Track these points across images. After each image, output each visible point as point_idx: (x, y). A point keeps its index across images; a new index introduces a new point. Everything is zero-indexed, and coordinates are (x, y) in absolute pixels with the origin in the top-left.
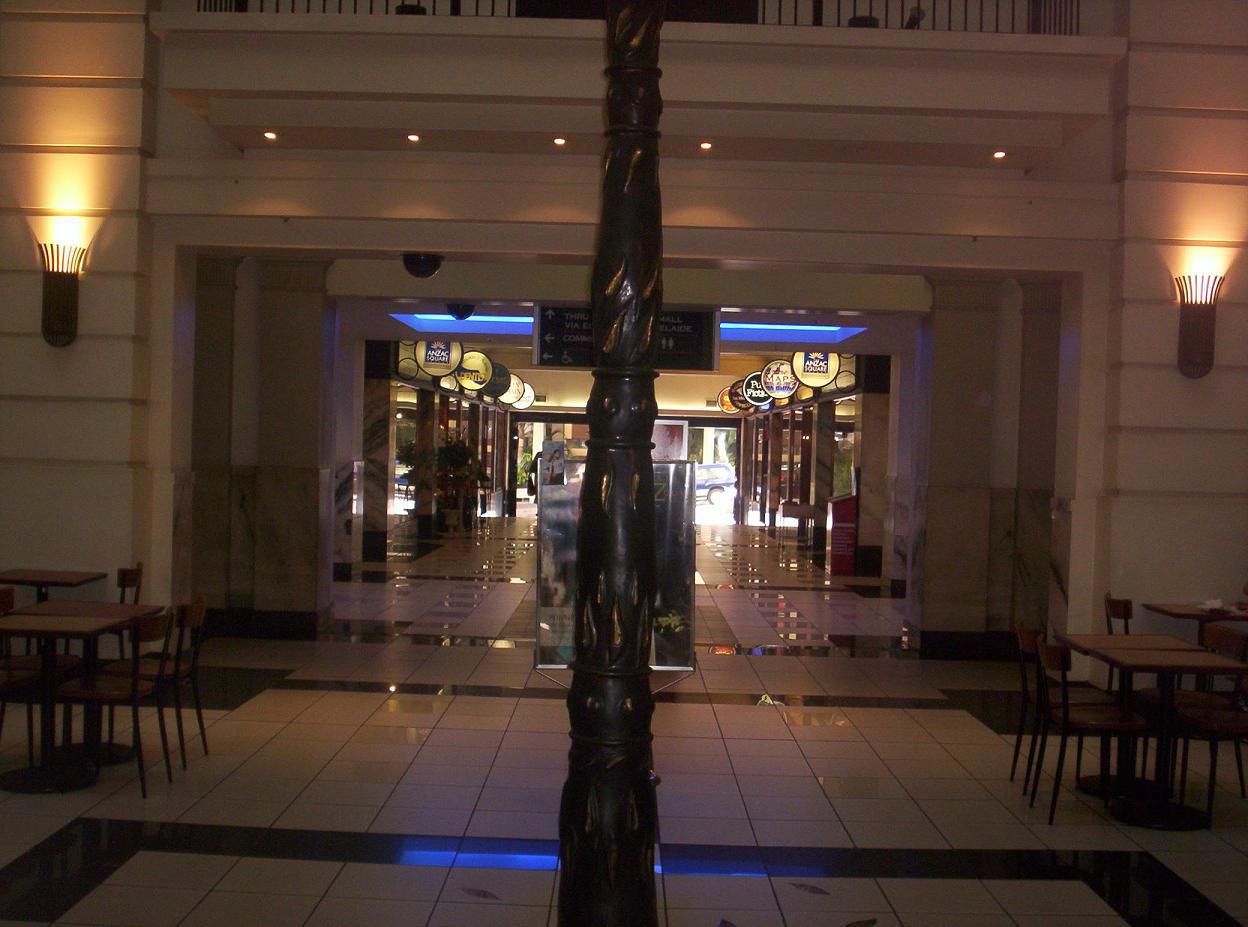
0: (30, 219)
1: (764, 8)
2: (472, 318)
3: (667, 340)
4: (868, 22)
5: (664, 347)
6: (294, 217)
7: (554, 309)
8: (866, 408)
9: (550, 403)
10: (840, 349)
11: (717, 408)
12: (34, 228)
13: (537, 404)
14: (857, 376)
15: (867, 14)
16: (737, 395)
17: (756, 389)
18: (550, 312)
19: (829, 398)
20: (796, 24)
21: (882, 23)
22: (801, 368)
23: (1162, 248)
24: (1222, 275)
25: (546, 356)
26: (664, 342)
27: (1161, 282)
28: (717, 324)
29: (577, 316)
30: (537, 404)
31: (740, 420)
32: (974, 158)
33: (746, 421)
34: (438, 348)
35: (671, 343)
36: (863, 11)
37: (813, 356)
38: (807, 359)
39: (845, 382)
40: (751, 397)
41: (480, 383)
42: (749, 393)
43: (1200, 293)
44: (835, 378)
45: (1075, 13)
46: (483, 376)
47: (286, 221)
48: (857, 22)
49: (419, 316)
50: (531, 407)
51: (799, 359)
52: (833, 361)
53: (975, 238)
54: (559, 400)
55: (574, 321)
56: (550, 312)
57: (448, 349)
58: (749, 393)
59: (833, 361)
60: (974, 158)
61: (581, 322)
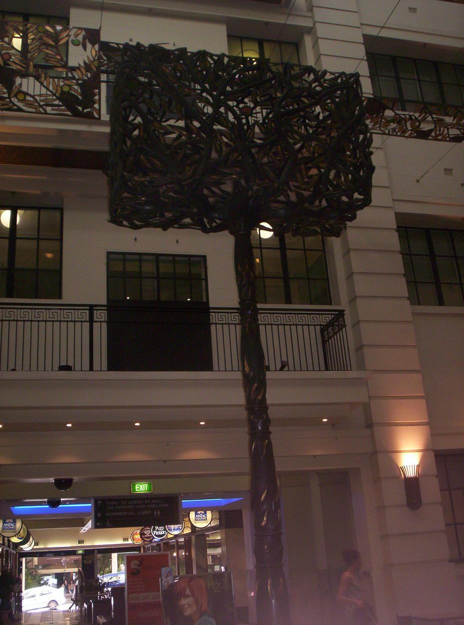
0: (392, 455)
1: (237, 347)
2: (60, 506)
3: (157, 511)
4: (67, 368)
5: (156, 515)
6: (6, 465)
7: (102, 500)
8: (227, 537)
9: (41, 546)
10: (212, 509)
11: (130, 542)
12: (396, 461)
13: (36, 547)
14: (220, 520)
15: (65, 364)
16: (145, 534)
17: (158, 531)
18: (99, 502)
19: (202, 533)
20: (37, 370)
21: (73, 369)
22: (194, 519)
23: (392, 454)
24: (418, 464)
25: (98, 524)
26: (155, 513)
27: (395, 470)
28: (180, 500)
29: (113, 503)
30: (36, 547)
31: (141, 547)
32: (129, 426)
33: (144, 547)
34: (10, 522)
35: (159, 513)
36: (63, 363)
37: (199, 512)
38: (196, 514)
39: (215, 523)
40: (155, 535)
41: (21, 539)
42: (154, 533)
43: (411, 473)
44: (210, 523)
45: (347, 352)
46: (22, 535)
47: (165, 462)
48: (63, 368)
49: (15, 507)
50: (33, 549)
51: (192, 515)
52: (209, 514)
53: (315, 456)
54: (45, 544)
55: (111, 505)
56: (99, 502)
57: (15, 522)
58: (154, 533)
59: (209, 514)
60: (191, 425)
61: (114, 506)
